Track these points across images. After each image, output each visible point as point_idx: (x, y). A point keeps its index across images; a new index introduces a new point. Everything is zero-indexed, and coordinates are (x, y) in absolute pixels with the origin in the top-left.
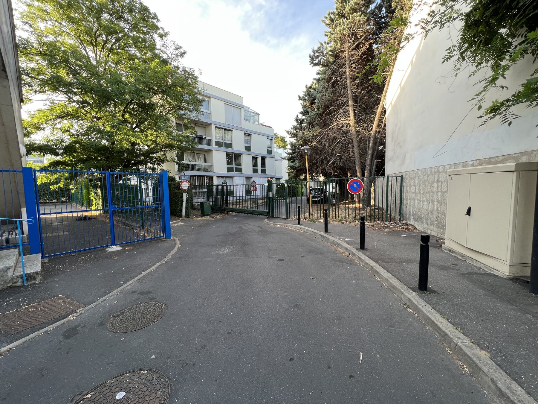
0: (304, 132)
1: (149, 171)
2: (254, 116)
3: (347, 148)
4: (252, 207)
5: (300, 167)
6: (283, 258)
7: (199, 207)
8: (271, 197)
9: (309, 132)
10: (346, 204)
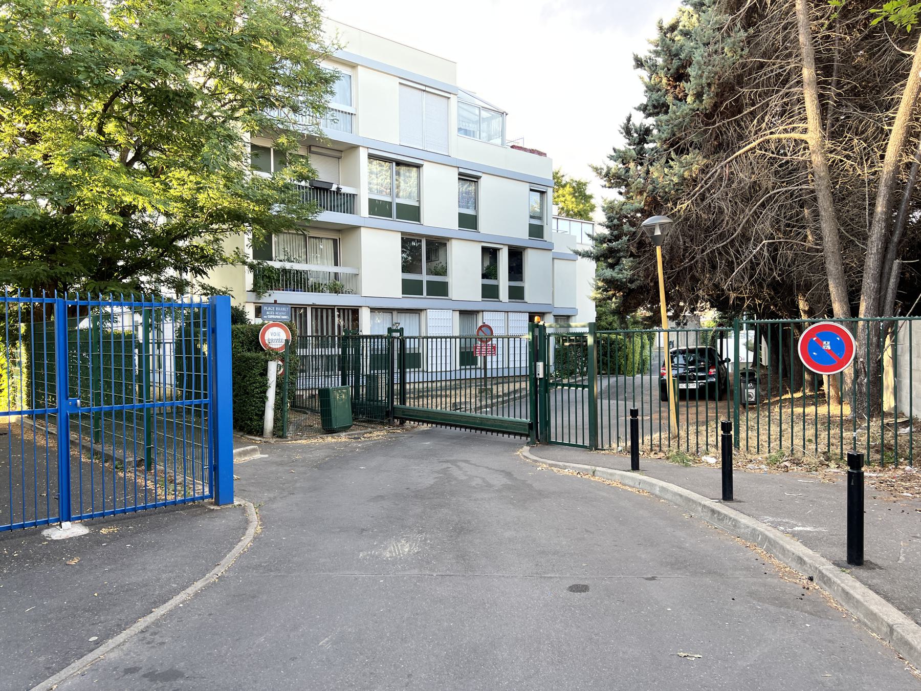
0: (651, 169)
1: (167, 292)
2: (488, 120)
3: (797, 221)
4: (481, 407)
5: (637, 283)
6: (586, 583)
7: (317, 404)
8: (541, 376)
9: (666, 170)
10: (792, 401)
